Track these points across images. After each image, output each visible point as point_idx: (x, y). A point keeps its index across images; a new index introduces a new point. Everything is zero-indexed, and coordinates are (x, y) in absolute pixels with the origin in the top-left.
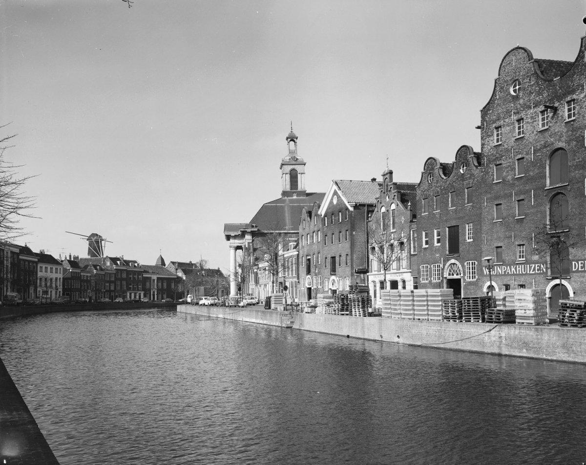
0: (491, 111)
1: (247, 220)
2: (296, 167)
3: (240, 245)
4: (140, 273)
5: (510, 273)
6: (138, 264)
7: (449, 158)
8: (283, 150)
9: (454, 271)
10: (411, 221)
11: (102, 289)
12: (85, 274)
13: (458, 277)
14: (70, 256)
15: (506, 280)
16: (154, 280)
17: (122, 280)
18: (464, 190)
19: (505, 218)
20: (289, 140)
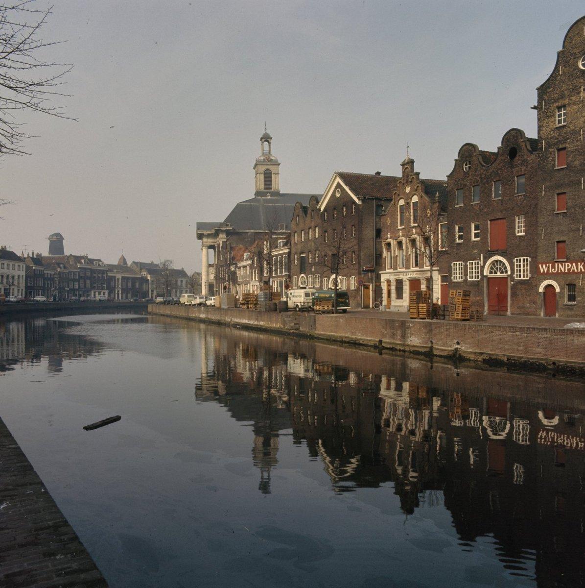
0: (551, 89)
1: (222, 220)
2: (270, 167)
3: (212, 244)
4: (104, 272)
5: (576, 271)
6: (103, 263)
7: (491, 143)
8: (256, 151)
9: (497, 269)
10: (440, 215)
11: (66, 287)
12: (49, 272)
13: (504, 275)
14: (33, 253)
15: (570, 279)
16: (118, 279)
17: (86, 278)
18: (513, 178)
19: (570, 208)
20: (263, 140)
